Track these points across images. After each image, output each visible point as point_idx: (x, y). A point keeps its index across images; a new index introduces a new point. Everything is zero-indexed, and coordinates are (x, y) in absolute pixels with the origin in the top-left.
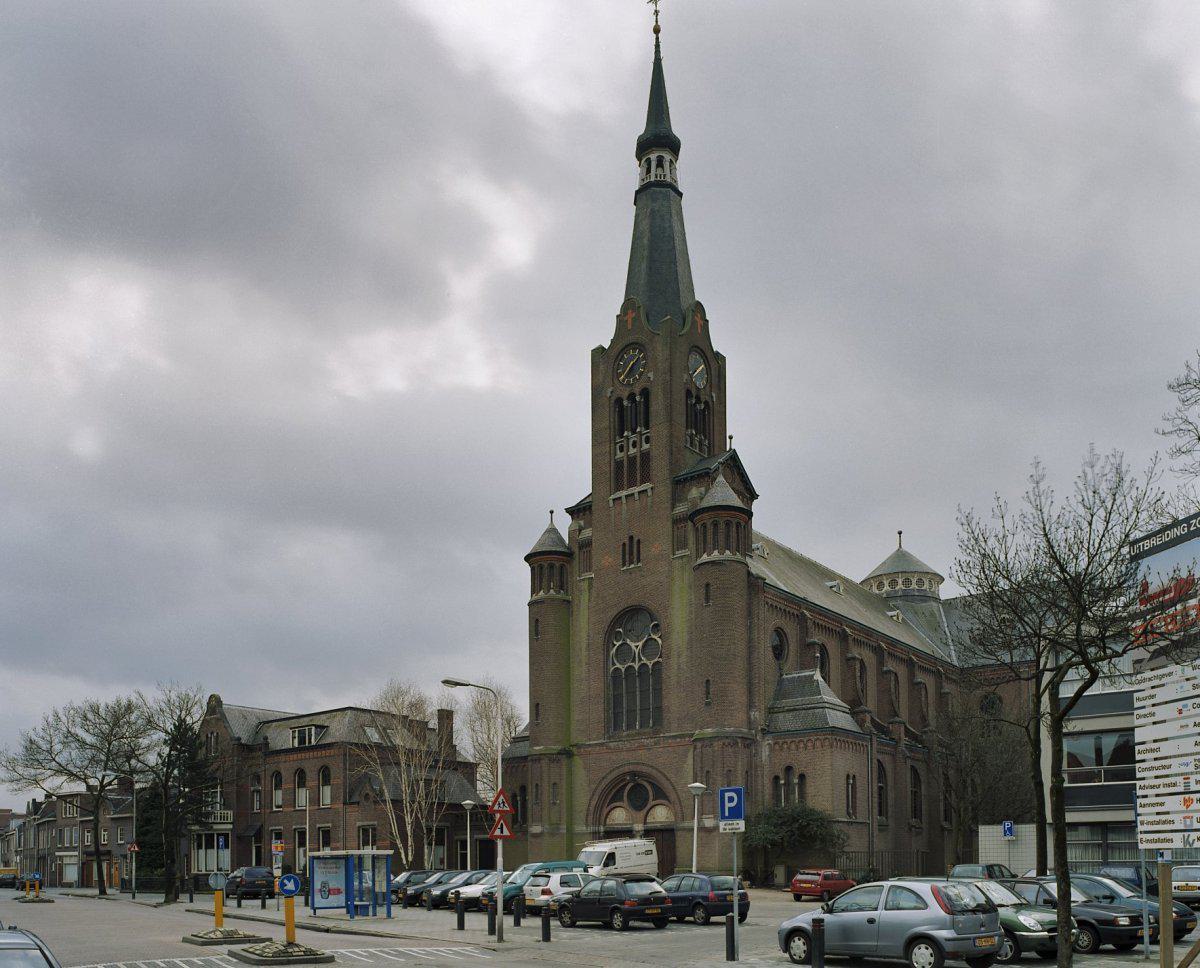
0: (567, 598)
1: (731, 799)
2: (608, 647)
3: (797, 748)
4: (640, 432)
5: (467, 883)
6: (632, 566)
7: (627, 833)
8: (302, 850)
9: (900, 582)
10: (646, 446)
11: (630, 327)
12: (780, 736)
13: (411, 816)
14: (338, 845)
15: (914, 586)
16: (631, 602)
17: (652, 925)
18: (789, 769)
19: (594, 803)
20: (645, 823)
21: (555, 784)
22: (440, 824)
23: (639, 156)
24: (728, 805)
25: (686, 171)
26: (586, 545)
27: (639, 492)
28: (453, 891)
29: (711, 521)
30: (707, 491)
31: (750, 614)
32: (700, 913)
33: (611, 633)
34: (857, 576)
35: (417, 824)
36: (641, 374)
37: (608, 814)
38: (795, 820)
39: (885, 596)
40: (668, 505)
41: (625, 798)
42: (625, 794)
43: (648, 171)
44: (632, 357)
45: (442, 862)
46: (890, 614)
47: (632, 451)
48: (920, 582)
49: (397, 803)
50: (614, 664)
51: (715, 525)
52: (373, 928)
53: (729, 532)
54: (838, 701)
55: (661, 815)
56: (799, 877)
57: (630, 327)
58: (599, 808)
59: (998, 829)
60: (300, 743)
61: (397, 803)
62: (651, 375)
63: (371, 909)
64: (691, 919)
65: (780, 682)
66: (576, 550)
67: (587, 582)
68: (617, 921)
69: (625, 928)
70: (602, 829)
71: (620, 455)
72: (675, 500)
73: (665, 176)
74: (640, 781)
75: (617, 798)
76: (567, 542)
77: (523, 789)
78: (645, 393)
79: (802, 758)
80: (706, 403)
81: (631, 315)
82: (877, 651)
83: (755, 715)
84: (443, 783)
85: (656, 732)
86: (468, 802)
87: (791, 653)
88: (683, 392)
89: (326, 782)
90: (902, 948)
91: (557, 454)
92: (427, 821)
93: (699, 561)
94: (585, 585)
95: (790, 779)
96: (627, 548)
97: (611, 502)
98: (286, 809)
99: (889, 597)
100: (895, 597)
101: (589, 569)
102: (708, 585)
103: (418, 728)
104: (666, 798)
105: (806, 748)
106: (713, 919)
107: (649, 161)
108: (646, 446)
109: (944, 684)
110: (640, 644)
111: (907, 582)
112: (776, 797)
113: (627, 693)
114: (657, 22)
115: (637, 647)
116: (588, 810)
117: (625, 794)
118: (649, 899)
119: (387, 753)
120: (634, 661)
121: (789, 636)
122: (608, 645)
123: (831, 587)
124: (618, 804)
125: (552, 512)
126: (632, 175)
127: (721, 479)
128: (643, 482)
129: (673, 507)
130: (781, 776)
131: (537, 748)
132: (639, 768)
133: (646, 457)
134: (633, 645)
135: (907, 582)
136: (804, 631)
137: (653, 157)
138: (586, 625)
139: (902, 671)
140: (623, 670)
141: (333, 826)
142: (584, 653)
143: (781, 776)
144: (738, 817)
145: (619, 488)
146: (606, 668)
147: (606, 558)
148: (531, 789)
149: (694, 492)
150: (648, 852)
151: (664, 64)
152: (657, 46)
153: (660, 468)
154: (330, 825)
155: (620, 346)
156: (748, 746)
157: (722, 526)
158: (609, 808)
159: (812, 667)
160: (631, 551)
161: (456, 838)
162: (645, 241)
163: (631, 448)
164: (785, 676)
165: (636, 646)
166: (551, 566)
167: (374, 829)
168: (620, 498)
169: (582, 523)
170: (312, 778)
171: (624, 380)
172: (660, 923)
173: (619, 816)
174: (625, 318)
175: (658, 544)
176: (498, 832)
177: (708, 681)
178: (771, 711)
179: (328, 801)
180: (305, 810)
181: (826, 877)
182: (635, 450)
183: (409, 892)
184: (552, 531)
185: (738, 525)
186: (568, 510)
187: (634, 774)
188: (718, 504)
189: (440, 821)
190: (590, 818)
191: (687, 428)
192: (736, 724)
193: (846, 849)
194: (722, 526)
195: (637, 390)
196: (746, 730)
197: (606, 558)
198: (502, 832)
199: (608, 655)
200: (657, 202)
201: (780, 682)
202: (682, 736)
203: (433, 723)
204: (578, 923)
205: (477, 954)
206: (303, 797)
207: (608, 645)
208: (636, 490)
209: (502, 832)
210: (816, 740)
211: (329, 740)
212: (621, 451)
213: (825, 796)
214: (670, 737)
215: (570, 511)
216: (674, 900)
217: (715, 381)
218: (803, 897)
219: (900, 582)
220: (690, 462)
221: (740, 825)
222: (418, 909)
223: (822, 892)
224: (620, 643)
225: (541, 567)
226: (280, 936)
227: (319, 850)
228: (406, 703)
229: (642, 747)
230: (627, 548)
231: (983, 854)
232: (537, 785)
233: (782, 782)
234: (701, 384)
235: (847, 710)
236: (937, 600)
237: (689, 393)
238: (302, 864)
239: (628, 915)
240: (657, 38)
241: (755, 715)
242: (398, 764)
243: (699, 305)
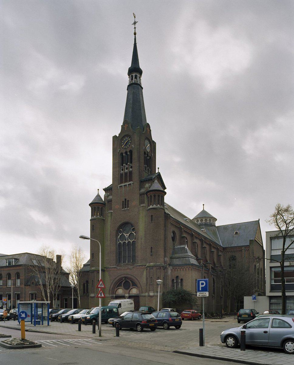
0: (103, 218)
1: (202, 284)
2: (117, 235)
3: (180, 270)
4: (129, 165)
5: (74, 313)
6: (126, 209)
7: (123, 297)
8: (9, 301)
9: (204, 220)
10: (131, 169)
11: (126, 129)
12: (175, 267)
13: (49, 290)
14: (22, 299)
15: (208, 221)
16: (125, 221)
17: (150, 330)
18: (177, 277)
19: (112, 287)
20: (129, 294)
22: (59, 293)
23: (129, 74)
24: (201, 286)
25: (144, 80)
26: (110, 201)
27: (129, 184)
28: (71, 316)
29: (153, 195)
30: (151, 185)
31: (165, 226)
32: (166, 325)
33: (118, 231)
34: (191, 218)
35: (51, 293)
36: (129, 145)
37: (116, 290)
38: (180, 294)
39: (199, 224)
40: (138, 189)
41: (122, 285)
42: (123, 284)
43: (132, 79)
44: (126, 140)
45: (59, 305)
46: (202, 230)
47: (126, 171)
48: (210, 220)
49: (44, 286)
50: (119, 241)
52: (41, 330)
53: (159, 198)
54: (193, 256)
55: (134, 291)
56: (184, 312)
57: (126, 129)
58: (113, 289)
59: (251, 298)
60: (9, 264)
61: (44, 286)
62: (133, 146)
63: (41, 322)
64: (163, 327)
65: (174, 249)
66: (106, 202)
67: (110, 214)
68: (139, 328)
69: (142, 331)
70: (114, 295)
71: (122, 172)
72: (141, 187)
73: (137, 81)
74: (127, 280)
75: (119, 285)
76: (103, 200)
77: (87, 282)
78: (131, 152)
79: (181, 273)
80: (150, 157)
81: (126, 125)
82: (201, 240)
83: (166, 259)
84: (60, 279)
85: (133, 264)
87: (177, 240)
88: (143, 152)
89: (18, 278)
90: (281, 342)
92: (54, 292)
93: (149, 208)
94: (110, 215)
95: (178, 280)
96: (124, 203)
97: (119, 187)
98: (4, 287)
99: (200, 225)
100: (202, 225)
101: (111, 209)
102: (152, 216)
103: (50, 261)
104: (136, 285)
106: (171, 327)
107: (132, 76)
108: (131, 169)
110: (128, 235)
111: (206, 220)
112: (173, 286)
113: (123, 251)
114: (135, 31)
115: (127, 236)
116: (110, 289)
117: (123, 284)
118: (150, 320)
119: (42, 269)
120: (126, 240)
121: (177, 234)
122: (117, 235)
123: (186, 220)
124: (120, 287)
125: (98, 190)
126: (126, 80)
127: (156, 181)
128: (130, 181)
129: (140, 190)
130: (175, 279)
132: (127, 276)
133: (131, 173)
135: (206, 220)
136: (181, 233)
137: (134, 75)
138: (110, 227)
139: (208, 247)
140: (131, 242)
141: (21, 293)
142: (109, 237)
143: (175, 279)
144: (206, 291)
145: (121, 183)
146: (116, 244)
147: (117, 206)
148: (90, 282)
149: (147, 185)
150: (131, 304)
151: (137, 45)
152: (135, 39)
153: (136, 176)
154: (20, 292)
155: (122, 136)
156: (164, 269)
157: (157, 197)
158: (117, 289)
159: (184, 244)
160: (126, 204)
161: (63, 298)
162: (131, 102)
163: (126, 169)
164: (175, 247)
165: (126, 235)
166: (98, 208)
167: (35, 294)
168: (122, 186)
169: (109, 194)
170: (13, 277)
171: (123, 147)
172: (153, 329)
173: (120, 291)
174: (124, 127)
175: (135, 202)
176: (100, 295)
177: (152, 247)
178: (171, 258)
179: (19, 284)
180: (11, 287)
181: (192, 312)
182: (127, 170)
183: (63, 317)
184: (98, 196)
186: (104, 189)
187: (126, 278)
188: (156, 189)
189: (59, 292)
190: (111, 292)
191: (144, 164)
192: (160, 262)
193: (197, 303)
194: (157, 197)
195: (128, 150)
196: (164, 264)
197: (117, 206)
198: (101, 295)
199: (117, 238)
200: (135, 90)
201: (174, 249)
202: (142, 266)
203: (55, 260)
204: (122, 329)
205: (94, 341)
206: (10, 283)
207: (117, 235)
208: (127, 184)
209: (101, 295)
210: (175, 269)
211: (20, 264)
212: (122, 171)
213: (188, 286)
214: (138, 266)
215: (105, 190)
216: (158, 320)
217: (153, 150)
218: (185, 319)
219: (204, 220)
220: (145, 175)
221: (207, 294)
222: (56, 322)
223: (191, 317)
224: (121, 234)
226: (17, 335)
227: (30, 301)
228: (48, 251)
229: (128, 269)
230: (124, 203)
231: (245, 304)
232: (93, 280)
233: (175, 281)
234: (148, 150)
235: (195, 259)
236: (215, 226)
237: (145, 153)
238: (9, 306)
239: (143, 326)
240: (135, 37)
241: (166, 259)
242: (45, 272)
243: (148, 124)
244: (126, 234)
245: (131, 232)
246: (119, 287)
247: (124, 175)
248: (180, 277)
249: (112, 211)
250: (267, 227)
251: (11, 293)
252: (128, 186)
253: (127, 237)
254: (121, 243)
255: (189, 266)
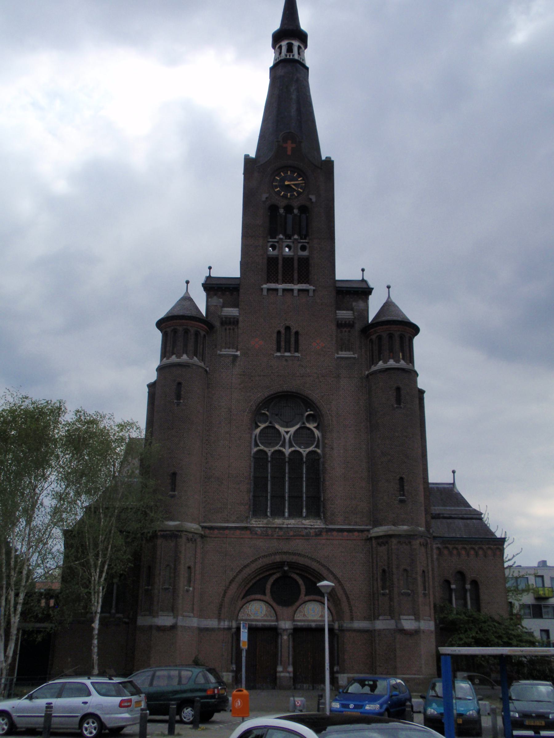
21: (189, 568)
27: (284, 290)
41: (268, 591)
51: (391, 336)
57: (289, 153)
62: (313, 198)
86: (325, 583)
91: (216, 243)
93: (374, 368)
105: (477, 555)
109: (137, 459)
110: (292, 430)
115: (287, 432)
120: (283, 445)
124: (258, 596)
125: (187, 282)
131: (172, 523)
134: (282, 430)
140: (269, 454)
165: (288, 432)
184: (187, 299)
185: (402, 337)
195: (296, 204)
214: (334, 530)
225: (175, 331)
244: (287, 427)
245: (304, 423)
246: (253, 597)
247: (280, 266)
248: (470, 576)
249: (238, 353)
250: (68, 417)
251: (96, 671)
252: (280, 293)
253: (287, 437)
254: (266, 453)
255: (495, 545)
